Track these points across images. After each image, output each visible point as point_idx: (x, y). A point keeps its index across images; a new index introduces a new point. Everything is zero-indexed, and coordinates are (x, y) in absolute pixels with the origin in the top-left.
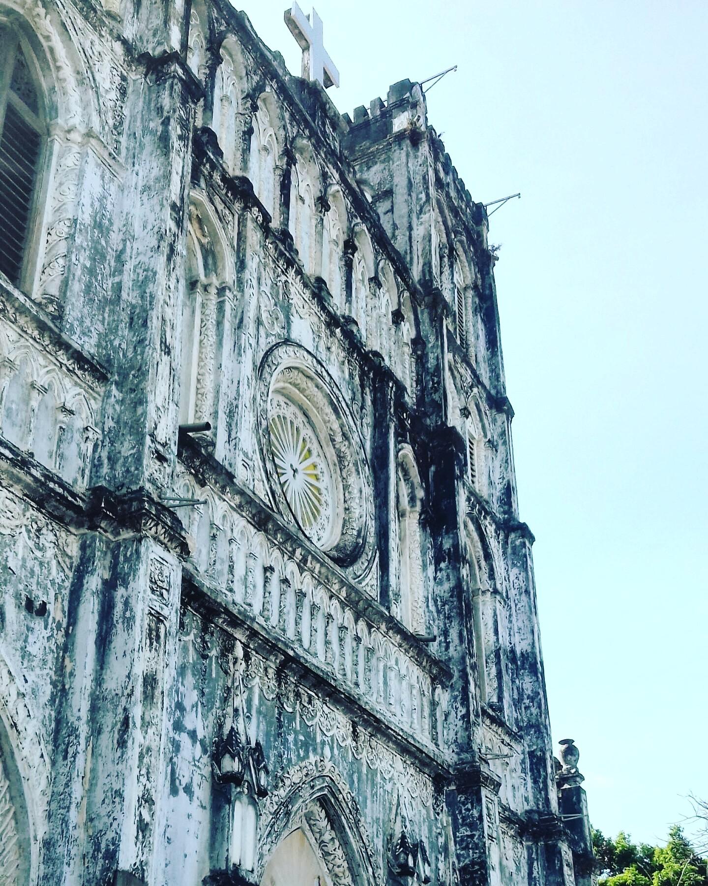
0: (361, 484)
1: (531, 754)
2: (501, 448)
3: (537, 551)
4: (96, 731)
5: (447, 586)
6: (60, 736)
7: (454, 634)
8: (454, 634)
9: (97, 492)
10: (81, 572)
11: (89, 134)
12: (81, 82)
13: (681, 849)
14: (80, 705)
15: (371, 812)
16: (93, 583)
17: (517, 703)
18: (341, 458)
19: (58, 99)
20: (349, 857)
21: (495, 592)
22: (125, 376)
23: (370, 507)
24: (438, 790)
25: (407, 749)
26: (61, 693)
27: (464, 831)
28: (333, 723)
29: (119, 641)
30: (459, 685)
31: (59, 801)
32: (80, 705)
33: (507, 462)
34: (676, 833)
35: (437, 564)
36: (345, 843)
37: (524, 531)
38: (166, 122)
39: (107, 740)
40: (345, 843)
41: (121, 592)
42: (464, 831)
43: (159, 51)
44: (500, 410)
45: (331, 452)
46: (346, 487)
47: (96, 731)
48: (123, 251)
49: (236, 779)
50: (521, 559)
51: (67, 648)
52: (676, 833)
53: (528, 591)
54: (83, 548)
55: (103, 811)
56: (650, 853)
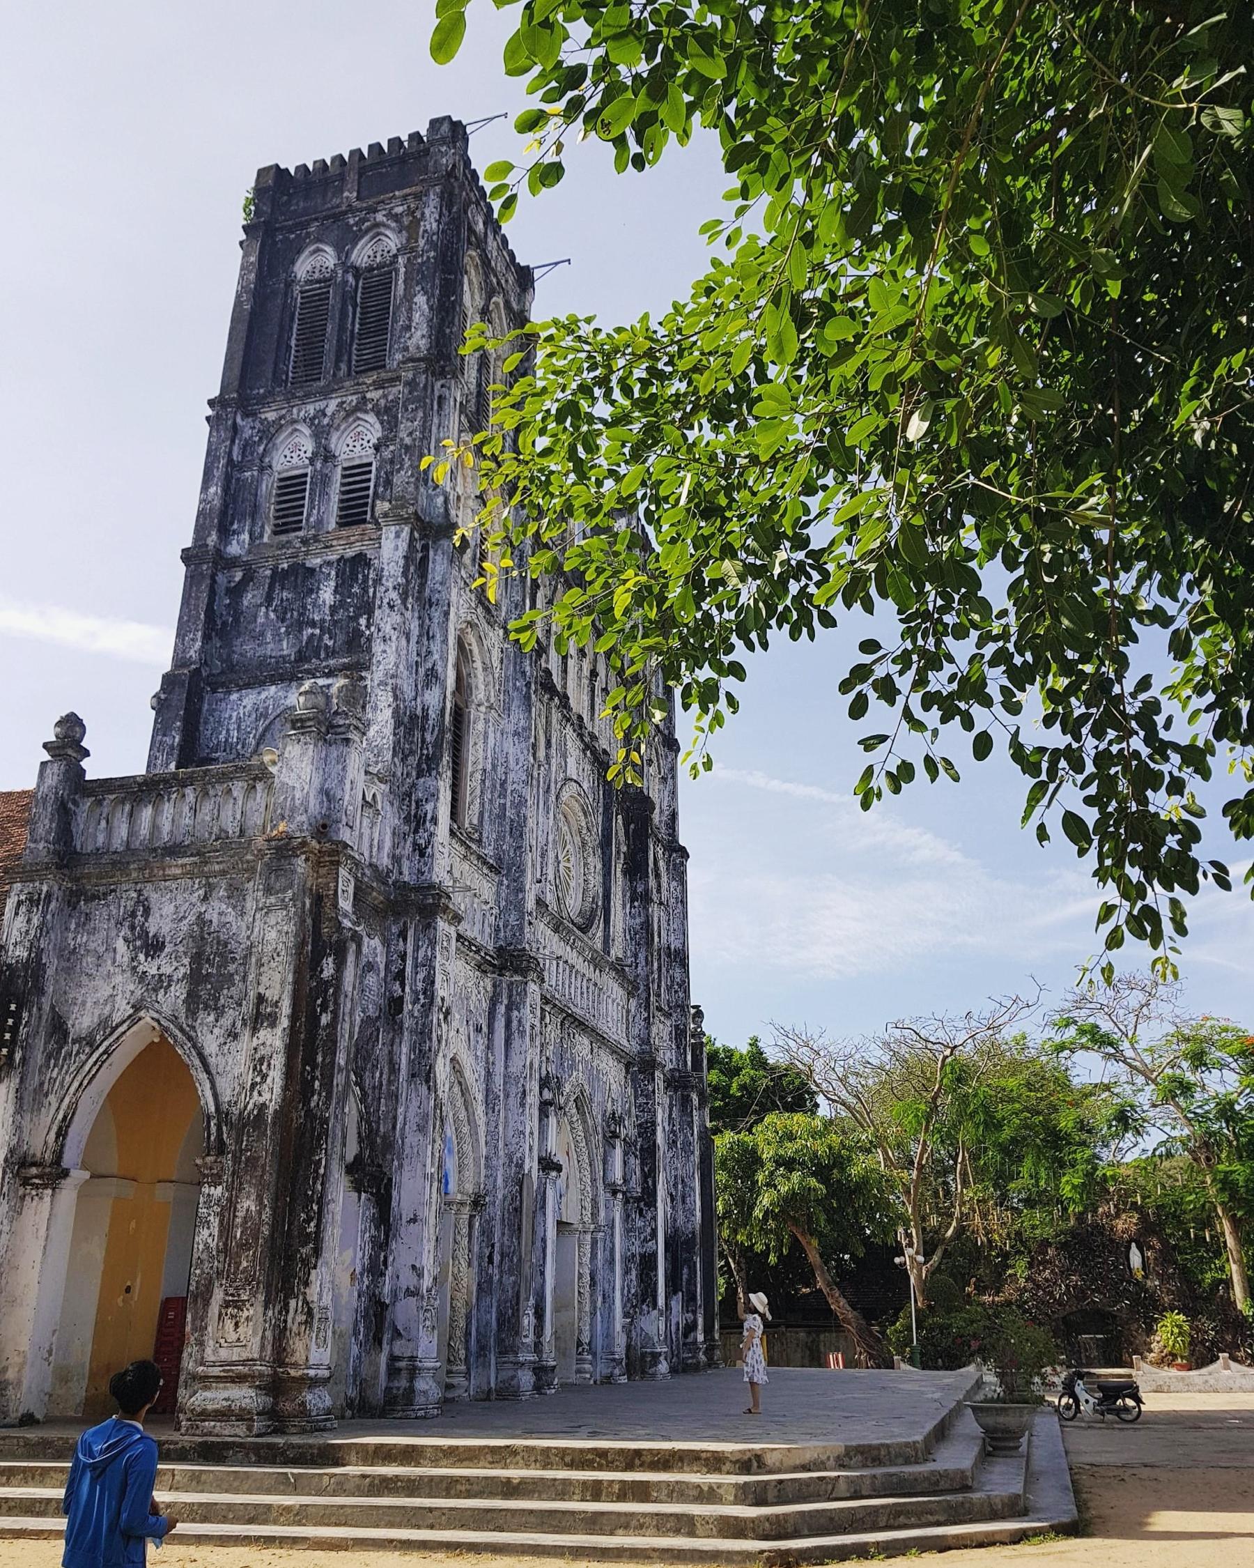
0: (595, 862)
1: (677, 1027)
2: (670, 781)
3: (690, 864)
4: (507, 1096)
5: (638, 921)
6: (490, 1101)
7: (641, 957)
8: (641, 957)
9: (500, 950)
10: (494, 1002)
11: (491, 707)
12: (485, 669)
13: (757, 1057)
14: (499, 1080)
15: (598, 1098)
16: (502, 1009)
17: (669, 988)
18: (584, 844)
19: (473, 681)
20: (586, 1131)
21: (661, 903)
22: (509, 870)
23: (600, 879)
24: (627, 1072)
25: (616, 1051)
26: (489, 1074)
27: (642, 1100)
28: (583, 1044)
29: (516, 1043)
30: (644, 996)
31: (492, 1134)
32: (499, 1080)
33: (674, 793)
34: (754, 1043)
35: (632, 902)
36: (584, 1122)
37: (684, 853)
38: (528, 685)
39: (513, 1102)
40: (584, 1122)
41: (515, 1013)
42: (642, 1100)
43: (767, 1120)
44: (670, 749)
45: (577, 839)
46: (586, 864)
47: (507, 1096)
48: (505, 781)
49: (550, 1103)
50: (680, 875)
51: (489, 1047)
52: (754, 1043)
53: (683, 902)
54: (494, 986)
55: (514, 1141)
56: (730, 1053)
